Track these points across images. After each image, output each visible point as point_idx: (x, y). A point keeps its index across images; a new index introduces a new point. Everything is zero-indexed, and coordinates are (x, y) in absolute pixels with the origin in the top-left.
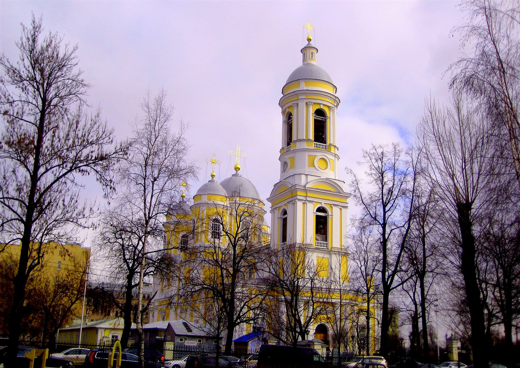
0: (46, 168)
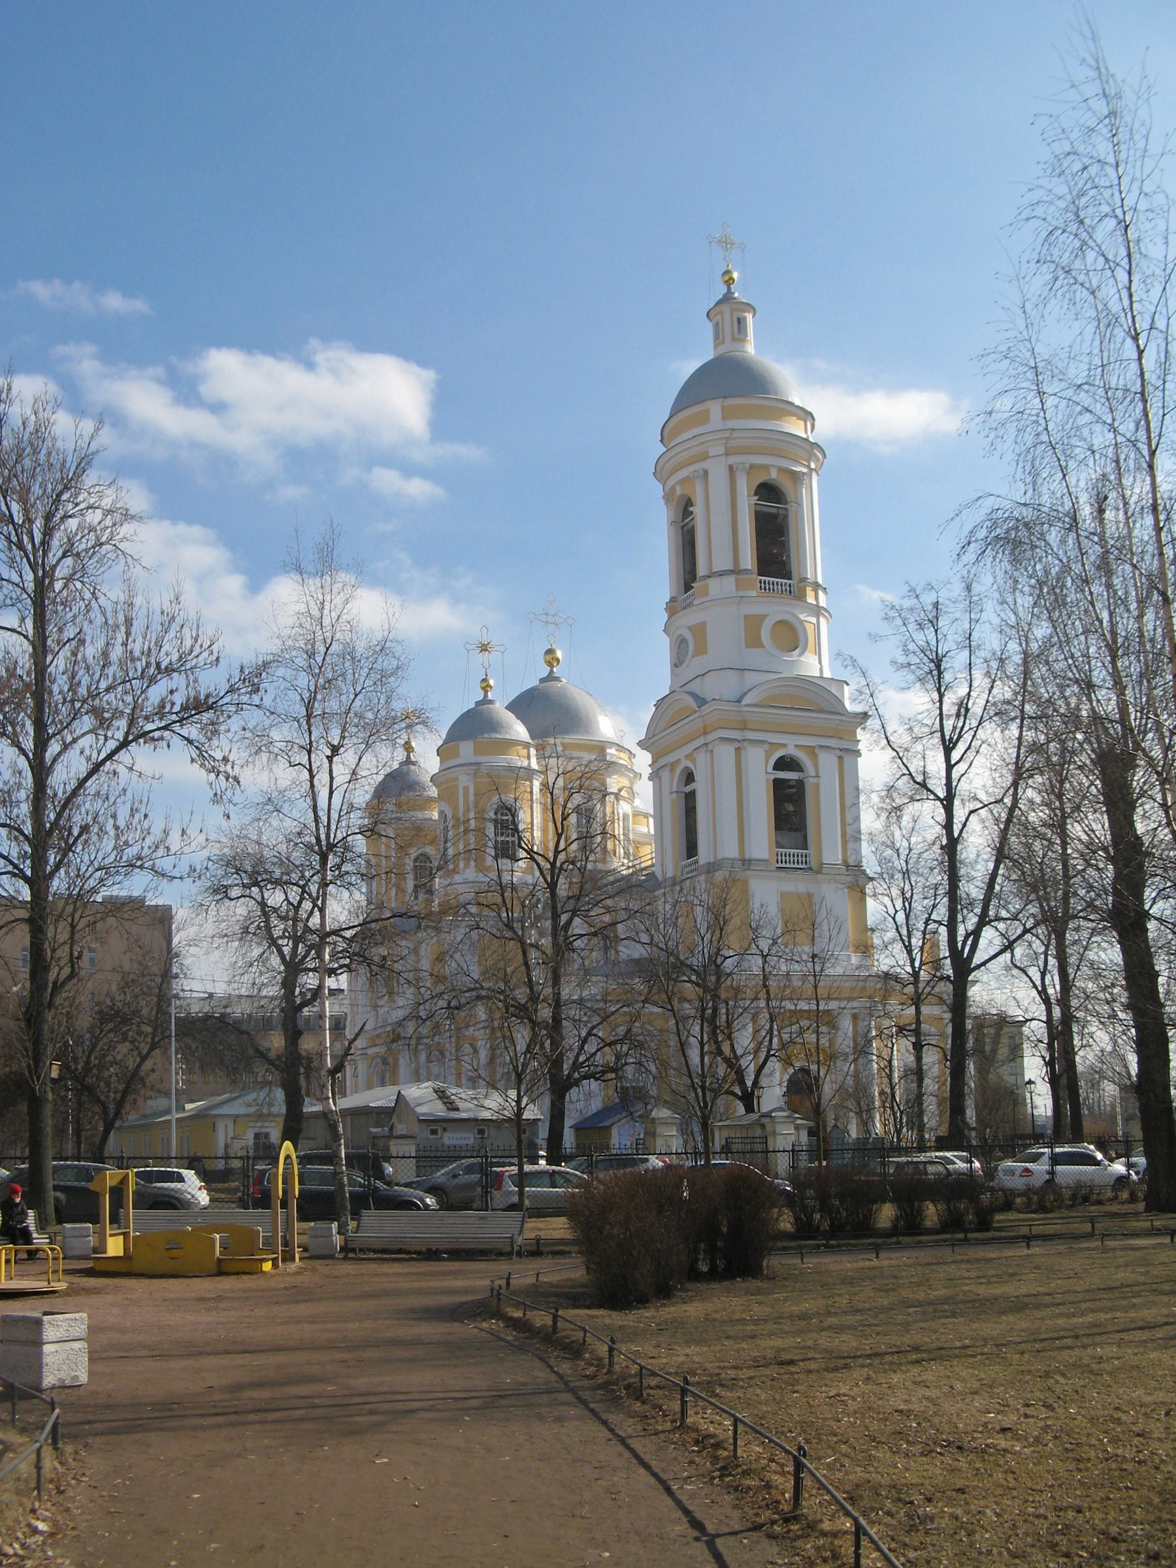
0: (64, 743)
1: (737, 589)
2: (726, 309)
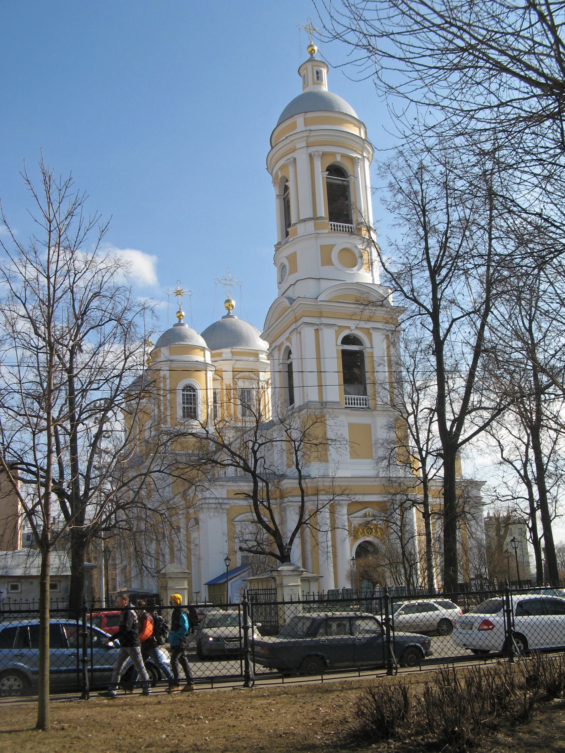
1: (315, 230)
2: (309, 66)
